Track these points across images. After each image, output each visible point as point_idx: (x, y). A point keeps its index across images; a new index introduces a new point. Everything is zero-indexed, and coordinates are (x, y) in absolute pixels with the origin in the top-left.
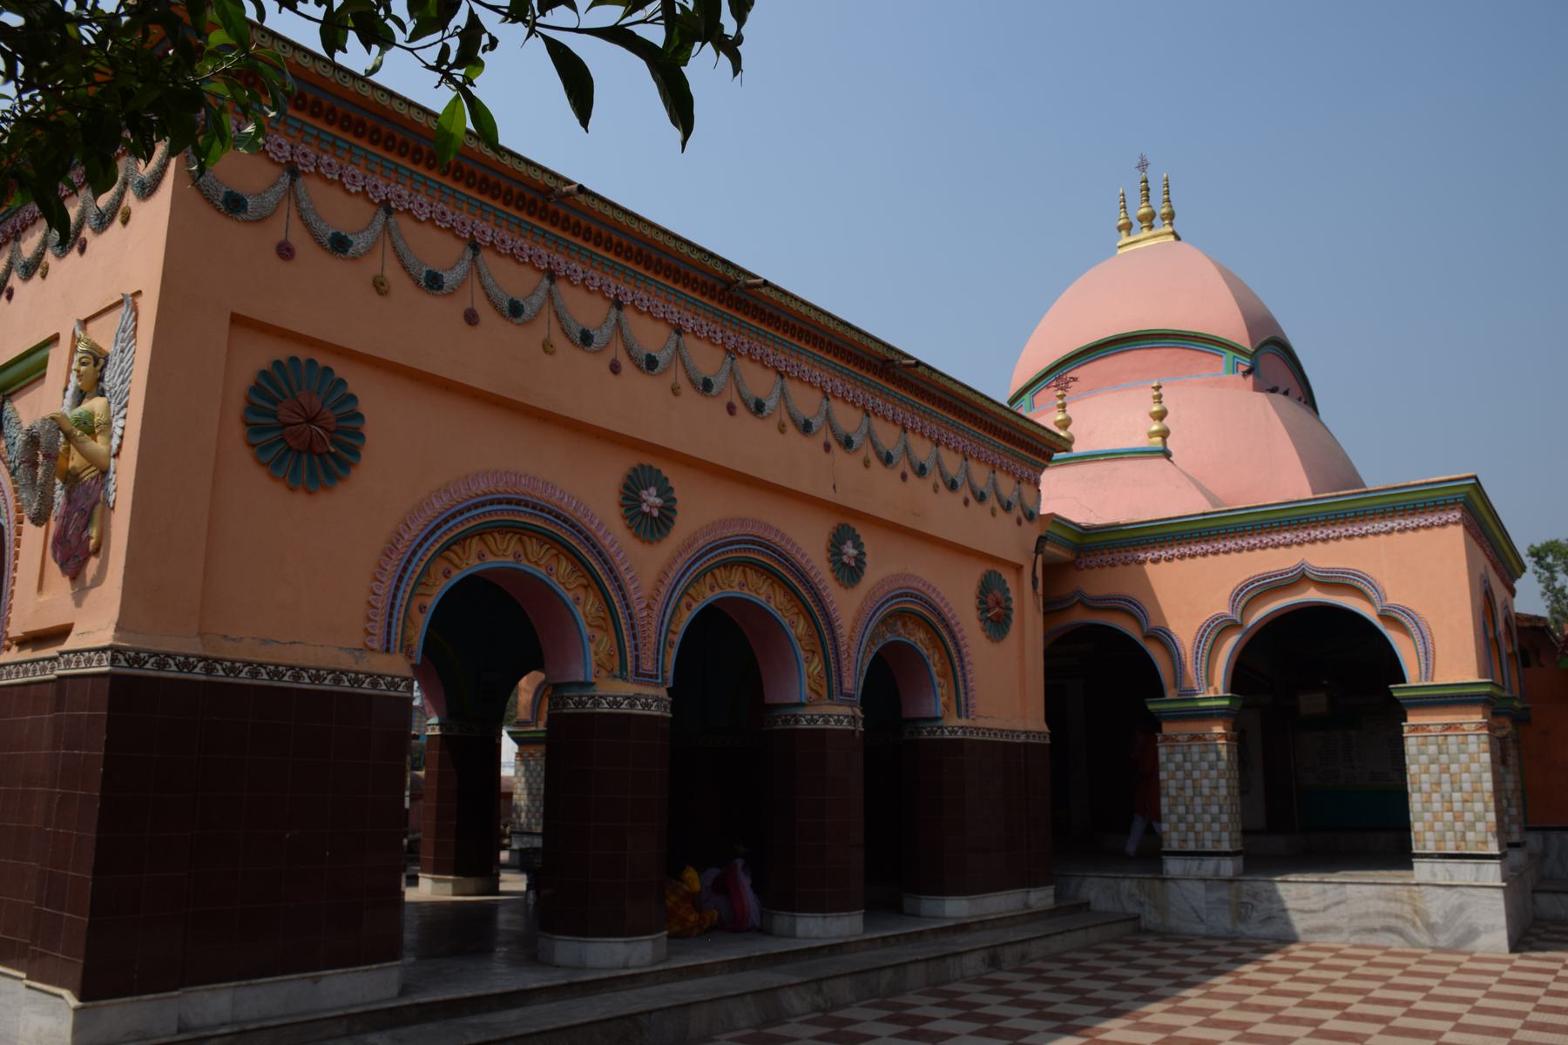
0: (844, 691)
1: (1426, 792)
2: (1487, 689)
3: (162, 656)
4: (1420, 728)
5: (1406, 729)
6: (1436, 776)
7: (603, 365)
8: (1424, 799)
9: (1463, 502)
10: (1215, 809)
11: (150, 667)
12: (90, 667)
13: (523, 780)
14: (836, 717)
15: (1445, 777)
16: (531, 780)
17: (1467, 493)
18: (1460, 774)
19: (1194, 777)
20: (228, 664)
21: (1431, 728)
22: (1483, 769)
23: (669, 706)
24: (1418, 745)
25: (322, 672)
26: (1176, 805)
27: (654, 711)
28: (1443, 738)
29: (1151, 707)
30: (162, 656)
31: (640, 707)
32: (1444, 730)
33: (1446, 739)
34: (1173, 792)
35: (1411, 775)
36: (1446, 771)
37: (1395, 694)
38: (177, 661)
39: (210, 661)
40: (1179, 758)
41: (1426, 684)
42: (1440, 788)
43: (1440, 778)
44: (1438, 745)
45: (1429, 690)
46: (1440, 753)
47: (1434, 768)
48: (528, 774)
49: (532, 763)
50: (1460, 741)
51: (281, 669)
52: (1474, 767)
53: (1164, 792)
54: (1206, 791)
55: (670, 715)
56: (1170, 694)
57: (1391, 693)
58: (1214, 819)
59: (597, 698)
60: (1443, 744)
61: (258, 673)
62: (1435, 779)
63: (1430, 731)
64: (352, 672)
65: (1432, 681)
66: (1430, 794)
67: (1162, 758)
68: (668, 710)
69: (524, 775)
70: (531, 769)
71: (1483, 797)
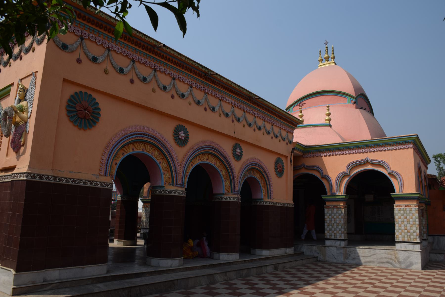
0: (236, 190)
2: (418, 195)
5: (395, 206)
6: (403, 219)
9: (413, 142)
10: (340, 227)
11: (88, 184)
12: (21, 178)
13: (145, 213)
14: (233, 198)
15: (405, 220)
16: (147, 213)
17: (415, 139)
19: (334, 218)
20: (73, 180)
22: (416, 218)
26: (338, 226)
27: (181, 195)
28: (405, 209)
29: (323, 198)
30: (41, 175)
34: (328, 222)
35: (396, 219)
37: (392, 196)
42: (404, 223)
43: (404, 220)
44: (404, 211)
46: (404, 213)
48: (146, 212)
49: (147, 208)
51: (220, 197)
52: (414, 217)
53: (326, 222)
54: (338, 222)
55: (186, 196)
56: (329, 194)
57: (391, 196)
61: (81, 182)
62: (402, 220)
63: (402, 207)
65: (403, 192)
66: (401, 225)
68: (185, 195)
69: (145, 212)
70: (147, 210)
71: (341, 224)
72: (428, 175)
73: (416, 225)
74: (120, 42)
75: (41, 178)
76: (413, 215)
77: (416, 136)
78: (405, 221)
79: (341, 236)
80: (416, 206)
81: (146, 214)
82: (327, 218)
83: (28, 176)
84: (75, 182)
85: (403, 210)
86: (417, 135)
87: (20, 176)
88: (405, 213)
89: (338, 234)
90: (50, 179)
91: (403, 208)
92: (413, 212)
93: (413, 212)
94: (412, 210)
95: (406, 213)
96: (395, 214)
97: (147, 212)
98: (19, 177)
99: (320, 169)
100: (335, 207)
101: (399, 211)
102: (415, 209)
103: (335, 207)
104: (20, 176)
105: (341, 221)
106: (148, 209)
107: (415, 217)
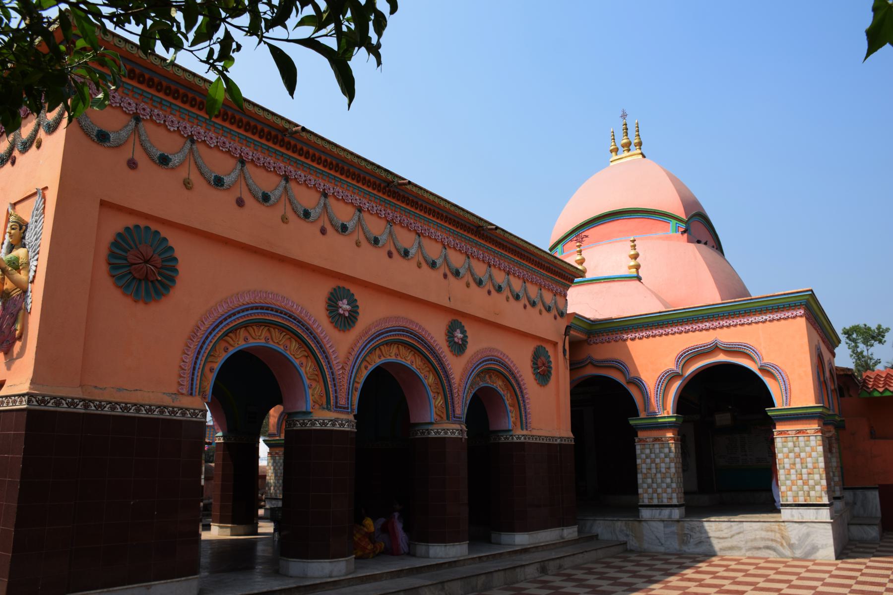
0: (456, 415)
1: (787, 469)
2: (820, 410)
3: (113, 404)
6: (793, 460)
10: (668, 480)
12: (15, 405)
13: (272, 468)
16: (277, 468)
20: (124, 405)
21: (808, 431)
22: (819, 456)
23: (355, 425)
24: (782, 442)
26: (646, 478)
27: (346, 428)
28: (796, 438)
30: (58, 399)
31: (338, 426)
32: (797, 434)
33: (798, 439)
34: (644, 471)
37: (769, 414)
39: (162, 408)
40: (648, 451)
42: (795, 466)
44: (794, 442)
45: (783, 411)
47: (791, 455)
48: (275, 464)
49: (277, 458)
50: (806, 440)
52: (814, 454)
53: (639, 471)
54: (663, 470)
55: (356, 430)
56: (642, 415)
57: (767, 413)
59: (162, 408)
60: (796, 442)
62: (792, 461)
63: (789, 434)
64: (192, 409)
67: (638, 452)
69: (273, 465)
70: (277, 461)
72: (837, 368)
73: (819, 470)
74: (246, 138)
75: (59, 403)
76: (813, 450)
78: (796, 462)
79: (671, 499)
81: (276, 470)
83: (89, 406)
85: (793, 440)
89: (665, 495)
90: (76, 406)
91: (793, 437)
92: (813, 443)
93: (813, 443)
94: (809, 441)
95: (799, 447)
96: (776, 449)
97: (277, 465)
98: (11, 405)
100: (656, 440)
101: (785, 442)
102: (816, 438)
103: (656, 440)
105: (669, 468)
106: (280, 459)
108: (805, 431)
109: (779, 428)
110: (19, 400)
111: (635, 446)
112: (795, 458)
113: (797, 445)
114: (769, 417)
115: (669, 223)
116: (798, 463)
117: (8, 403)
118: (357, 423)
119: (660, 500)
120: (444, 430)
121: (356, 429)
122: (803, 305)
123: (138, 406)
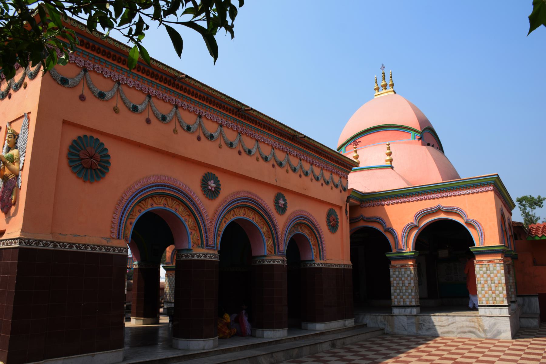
1: (482, 284)
2: (503, 248)
4: (491, 261)
6: (486, 278)
7: (143, 119)
8: (482, 286)
10: (410, 291)
12: (12, 245)
13: (168, 283)
17: (495, 180)
18: (494, 278)
21: (495, 261)
23: (218, 257)
25: (65, 244)
26: (396, 290)
27: (213, 259)
30: (71, 244)
31: (208, 258)
32: (500, 262)
34: (395, 285)
36: (489, 276)
37: (471, 250)
38: (43, 243)
41: (482, 246)
44: (486, 267)
48: (169, 281)
49: (171, 277)
50: (480, 267)
53: (392, 285)
54: (407, 285)
55: (219, 260)
56: (394, 251)
57: (470, 250)
58: (410, 294)
62: (485, 279)
63: (483, 263)
64: (119, 247)
69: (168, 282)
71: (411, 288)
75: (38, 244)
76: (498, 272)
77: (497, 176)
78: (488, 280)
80: (501, 261)
81: (170, 285)
82: (493, 276)
84: (110, 250)
86: (497, 175)
87: (11, 243)
88: (488, 270)
89: (407, 300)
90: (49, 246)
92: (498, 268)
93: (498, 268)
97: (171, 282)
99: (383, 221)
100: (402, 266)
101: (481, 267)
102: (500, 265)
103: (402, 266)
104: (11, 243)
105: (410, 283)
107: (501, 275)
108: (493, 261)
109: (478, 259)
110: (6, 243)
111: (390, 270)
112: (487, 277)
113: (488, 269)
114: (387, 258)
115: (410, 133)
116: (489, 280)
117: (7, 244)
118: (219, 256)
119: (405, 303)
120: (273, 260)
121: (219, 259)
122: (492, 183)
123: (86, 245)
